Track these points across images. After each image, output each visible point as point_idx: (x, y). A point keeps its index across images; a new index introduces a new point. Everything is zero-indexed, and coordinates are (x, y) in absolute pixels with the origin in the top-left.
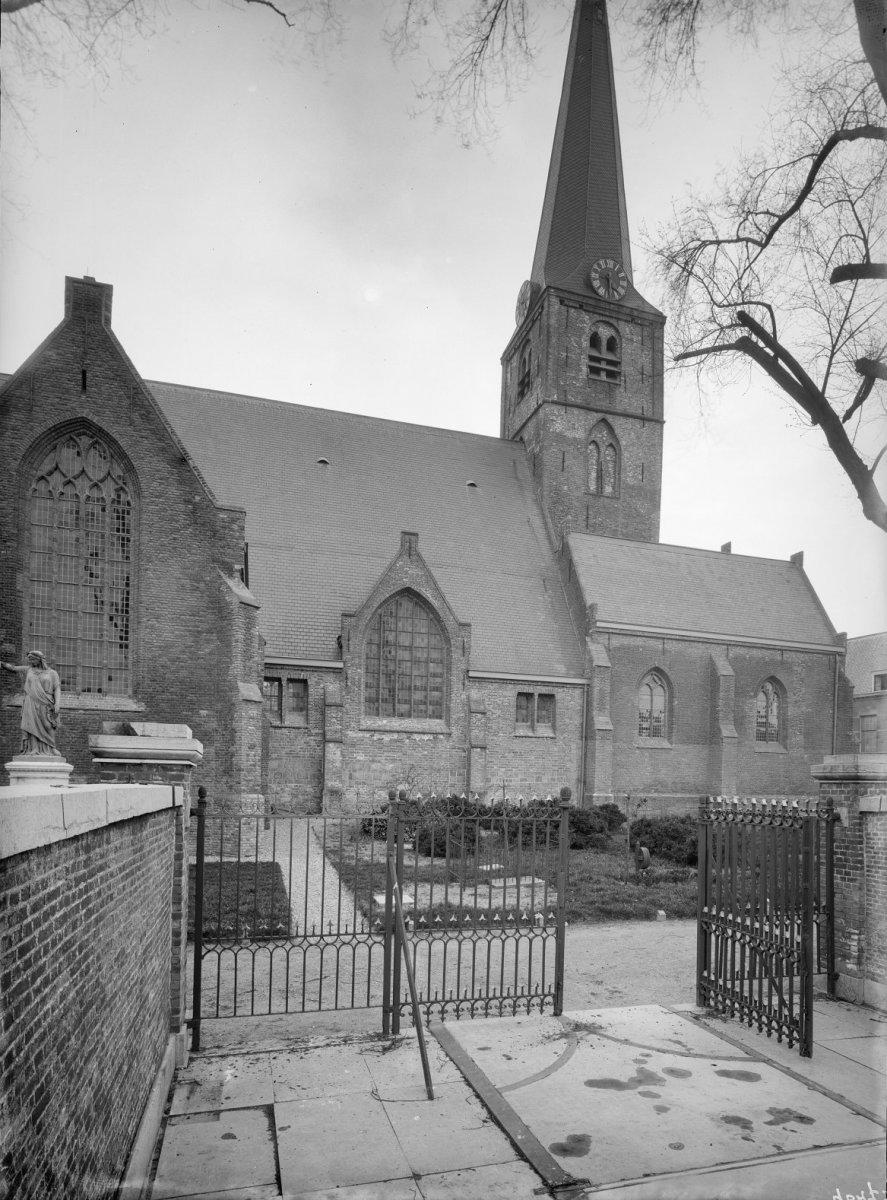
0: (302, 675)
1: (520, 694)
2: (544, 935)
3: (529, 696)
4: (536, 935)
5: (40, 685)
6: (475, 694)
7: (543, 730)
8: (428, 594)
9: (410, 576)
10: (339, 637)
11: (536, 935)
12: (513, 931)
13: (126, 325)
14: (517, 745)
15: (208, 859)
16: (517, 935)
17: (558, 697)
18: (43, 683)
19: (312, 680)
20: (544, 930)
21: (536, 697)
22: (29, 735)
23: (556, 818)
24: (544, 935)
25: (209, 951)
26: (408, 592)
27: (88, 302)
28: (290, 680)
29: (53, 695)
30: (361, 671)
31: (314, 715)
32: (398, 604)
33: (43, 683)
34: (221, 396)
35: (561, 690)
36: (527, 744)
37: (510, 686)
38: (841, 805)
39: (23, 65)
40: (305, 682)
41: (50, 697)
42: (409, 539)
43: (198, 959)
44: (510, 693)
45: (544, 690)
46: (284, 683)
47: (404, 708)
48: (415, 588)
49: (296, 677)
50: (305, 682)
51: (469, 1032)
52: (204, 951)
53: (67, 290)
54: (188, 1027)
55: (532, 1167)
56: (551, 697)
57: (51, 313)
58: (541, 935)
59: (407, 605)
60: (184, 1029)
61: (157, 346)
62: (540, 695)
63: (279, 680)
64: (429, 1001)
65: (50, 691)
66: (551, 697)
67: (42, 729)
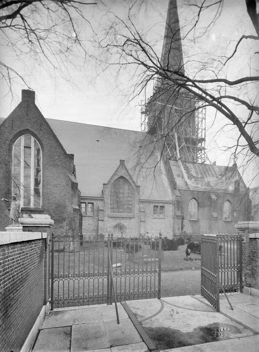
0: (92, 202)
1: (154, 206)
2: (155, 275)
3: (157, 206)
4: (152, 275)
5: (15, 205)
6: (141, 206)
7: (161, 216)
8: (127, 178)
9: (122, 173)
10: (103, 190)
11: (152, 275)
12: (146, 274)
13: (40, 102)
14: (154, 221)
15: (225, 254)
16: (143, 276)
17: (165, 207)
18: (16, 205)
19: (95, 203)
20: (143, 274)
21: (159, 207)
22: (12, 219)
23: (157, 241)
24: (134, 276)
25: (56, 281)
26: (122, 177)
27: (29, 96)
28: (89, 203)
29: (19, 208)
30: (109, 200)
31: (96, 213)
32: (119, 181)
33: (16, 205)
34: (78, 124)
35: (166, 205)
36: (157, 220)
37: (152, 204)
38: (244, 236)
39: (96, 67)
40: (93, 203)
41: (18, 208)
42: (122, 162)
43: (53, 283)
44: (152, 206)
45: (162, 205)
46: (87, 204)
47: (122, 210)
48: (124, 176)
49: (90, 202)
50: (93, 203)
51: (132, 304)
52: (54, 281)
53: (22, 94)
54: (50, 303)
55: (145, 343)
56: (164, 207)
57: (18, 99)
58: (154, 275)
59: (121, 180)
60: (48, 304)
61: (48, 107)
62: (160, 206)
63: (85, 203)
64: (63, 300)
65: (18, 207)
66: (164, 207)
67: (16, 218)
